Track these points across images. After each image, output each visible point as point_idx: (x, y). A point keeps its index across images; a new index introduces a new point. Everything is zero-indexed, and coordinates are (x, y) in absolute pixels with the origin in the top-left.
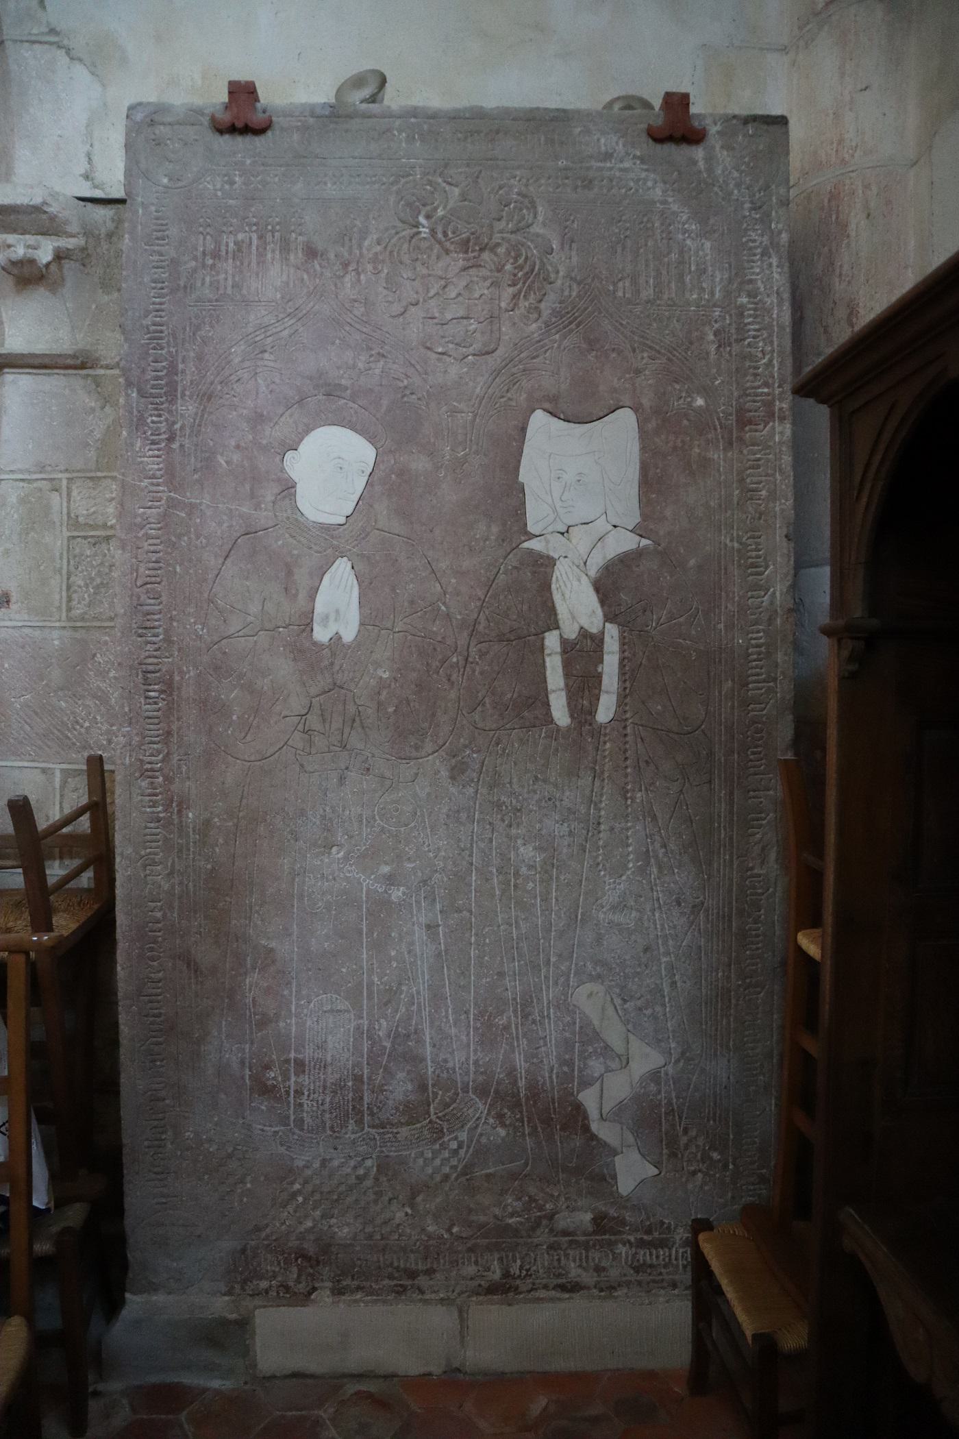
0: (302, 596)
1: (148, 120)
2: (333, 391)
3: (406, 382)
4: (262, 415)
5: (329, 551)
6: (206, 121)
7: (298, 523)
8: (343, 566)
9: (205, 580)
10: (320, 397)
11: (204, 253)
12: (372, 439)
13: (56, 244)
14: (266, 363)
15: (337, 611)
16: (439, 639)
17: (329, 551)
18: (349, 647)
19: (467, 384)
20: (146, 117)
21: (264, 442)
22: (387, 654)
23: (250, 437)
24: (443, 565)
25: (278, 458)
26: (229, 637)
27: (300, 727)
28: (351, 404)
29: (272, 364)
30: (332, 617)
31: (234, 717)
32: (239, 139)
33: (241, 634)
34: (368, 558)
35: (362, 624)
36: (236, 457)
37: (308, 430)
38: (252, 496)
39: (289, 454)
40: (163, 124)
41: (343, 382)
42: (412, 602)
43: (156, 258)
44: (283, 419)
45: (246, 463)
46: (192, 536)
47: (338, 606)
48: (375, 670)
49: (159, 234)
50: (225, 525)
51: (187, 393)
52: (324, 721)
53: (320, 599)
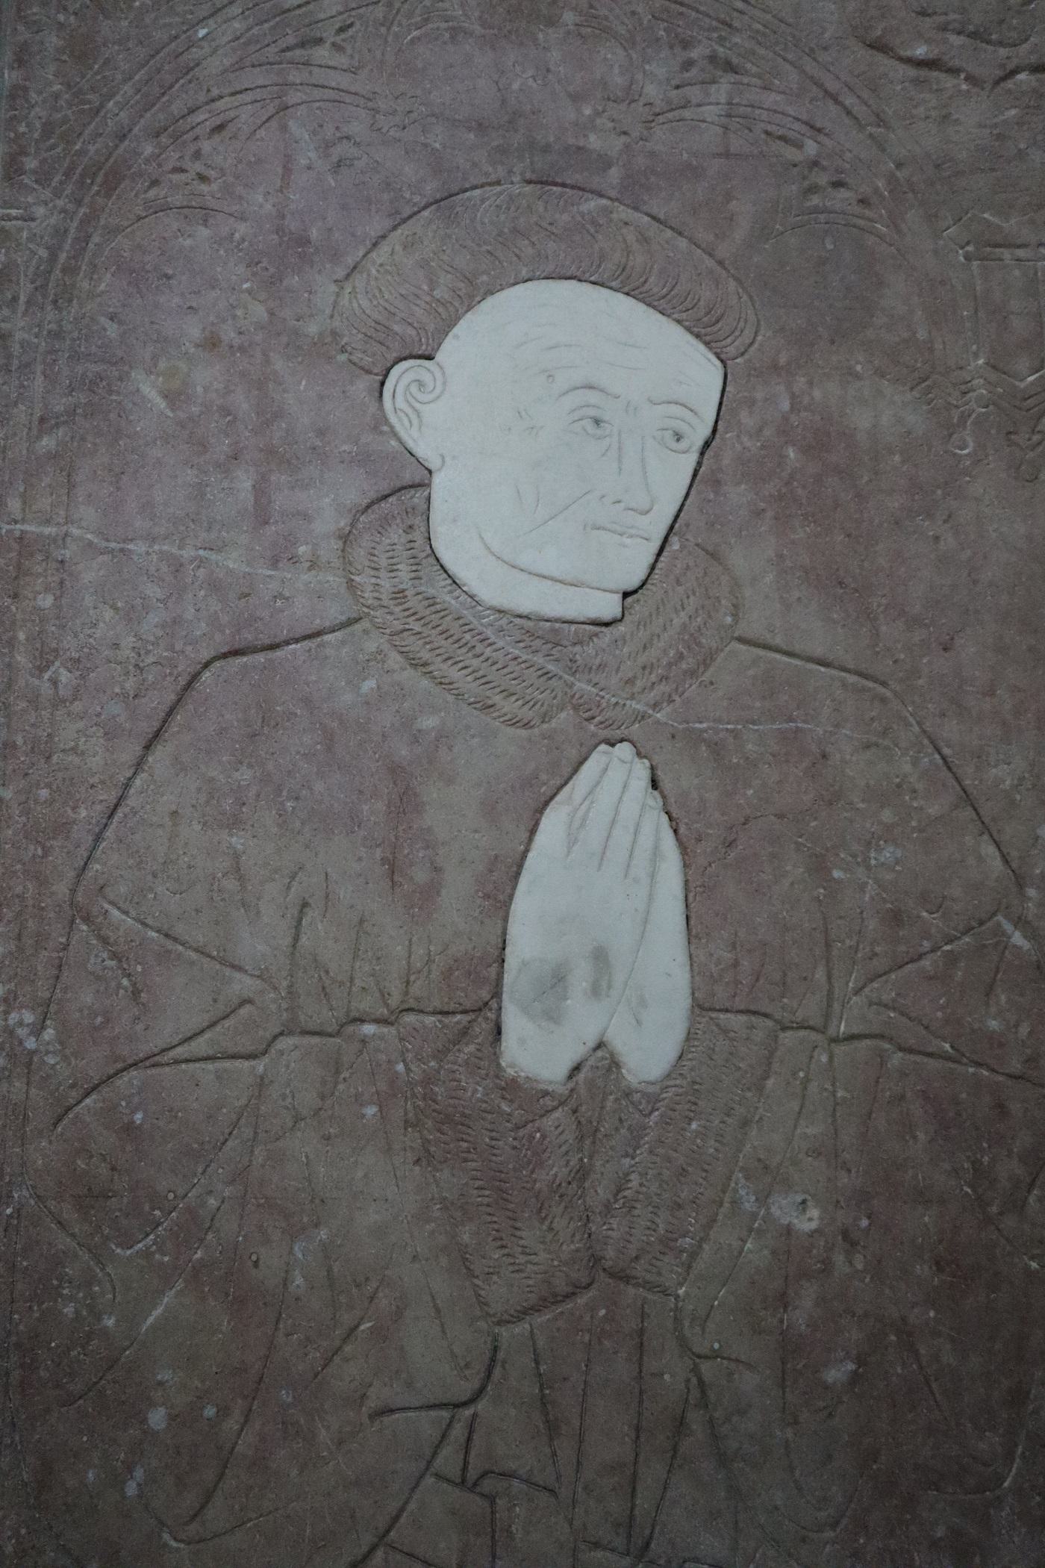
0: (458, 888)
2: (557, 172)
3: (811, 148)
4: (304, 241)
5: (564, 718)
7: (437, 618)
9: (63, 828)
12: (705, 329)
14: (319, 75)
15: (600, 957)
16: (1016, 1066)
18: (653, 1100)
19: (1021, 155)
21: (312, 329)
22: (813, 1129)
23: (259, 311)
24: (1003, 774)
25: (362, 386)
26: (149, 1061)
27: (448, 1459)
28: (623, 213)
29: (344, 80)
30: (580, 978)
31: (157, 1418)
33: (200, 1046)
34: (717, 749)
35: (700, 1007)
36: (206, 377)
37: (473, 292)
39: (403, 375)
41: (594, 142)
42: (896, 918)
45: (243, 403)
46: (21, 659)
47: (602, 933)
48: (763, 1199)
51: (31, 163)
52: (553, 1428)
53: (524, 905)
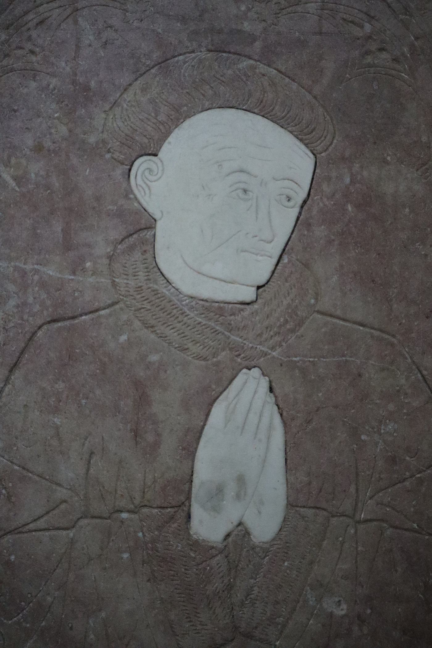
3: (368, 28)
4: (87, 89)
7: (160, 302)
8: (252, 385)
10: (203, 54)
12: (305, 135)
15: (241, 480)
17: (223, 356)
18: (266, 551)
21: (92, 139)
23: (64, 130)
25: (119, 172)
28: (262, 68)
30: (230, 491)
33: (41, 523)
35: (291, 505)
36: (36, 169)
37: (179, 116)
38: (67, 246)
41: (246, 26)
42: (393, 460)
44: (129, 96)
45: (56, 182)
48: (319, 600)
50: (12, 303)
53: (205, 453)
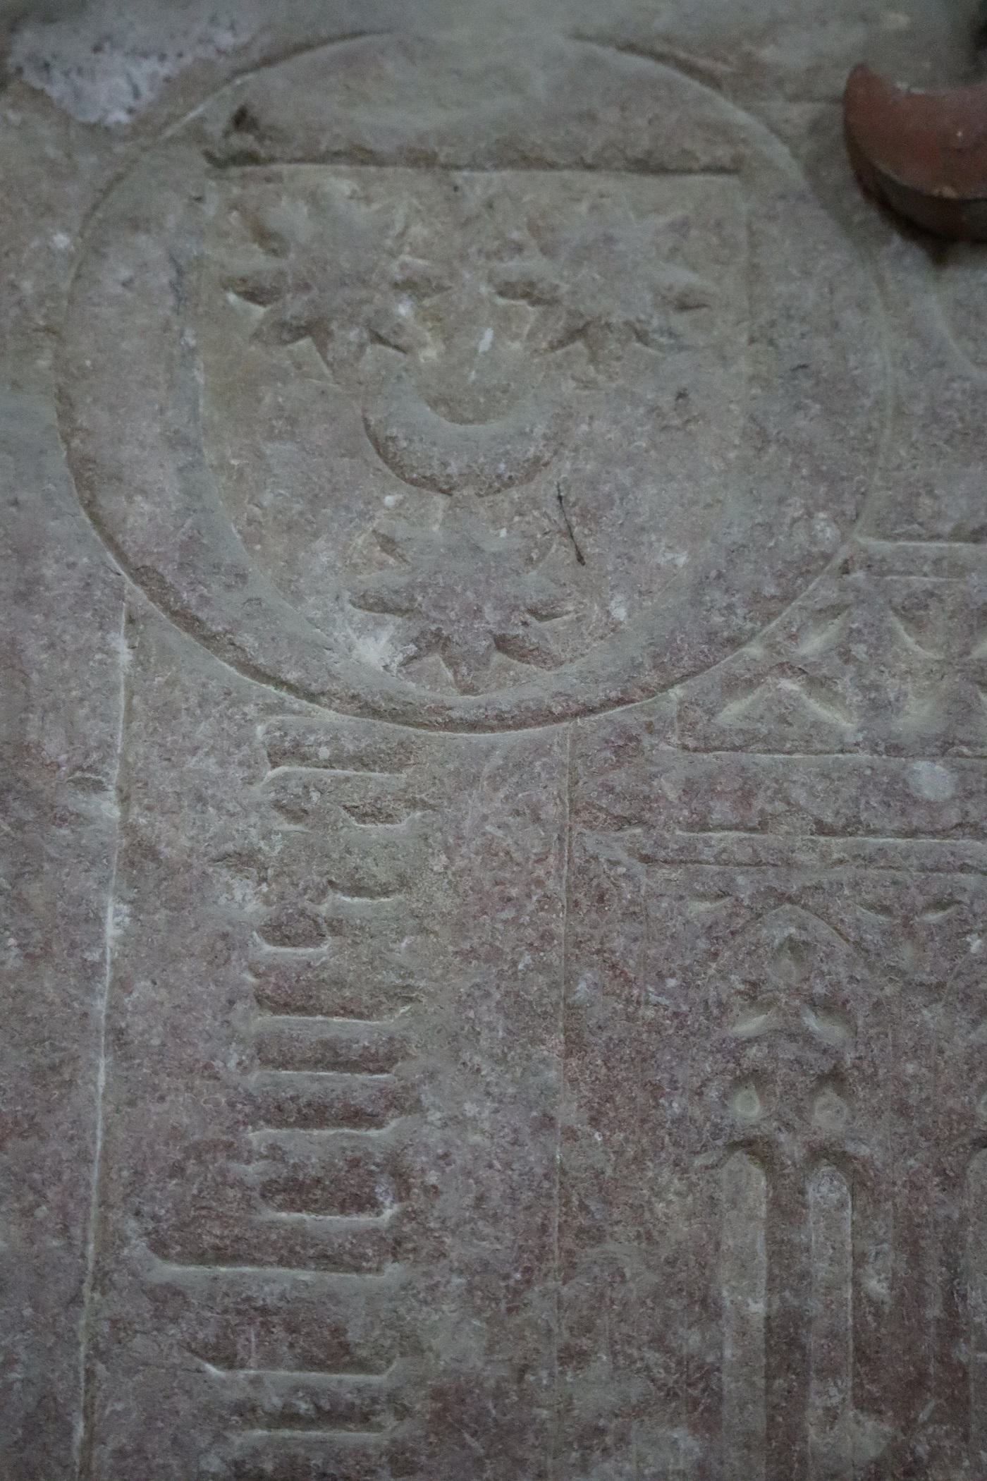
1: (213, 113)
6: (778, 138)
11: (785, 1340)
13: (377, 1219)
20: (180, 88)
32: (650, 180)
40: (359, 156)
43: (278, 1382)
49: (313, 1147)
